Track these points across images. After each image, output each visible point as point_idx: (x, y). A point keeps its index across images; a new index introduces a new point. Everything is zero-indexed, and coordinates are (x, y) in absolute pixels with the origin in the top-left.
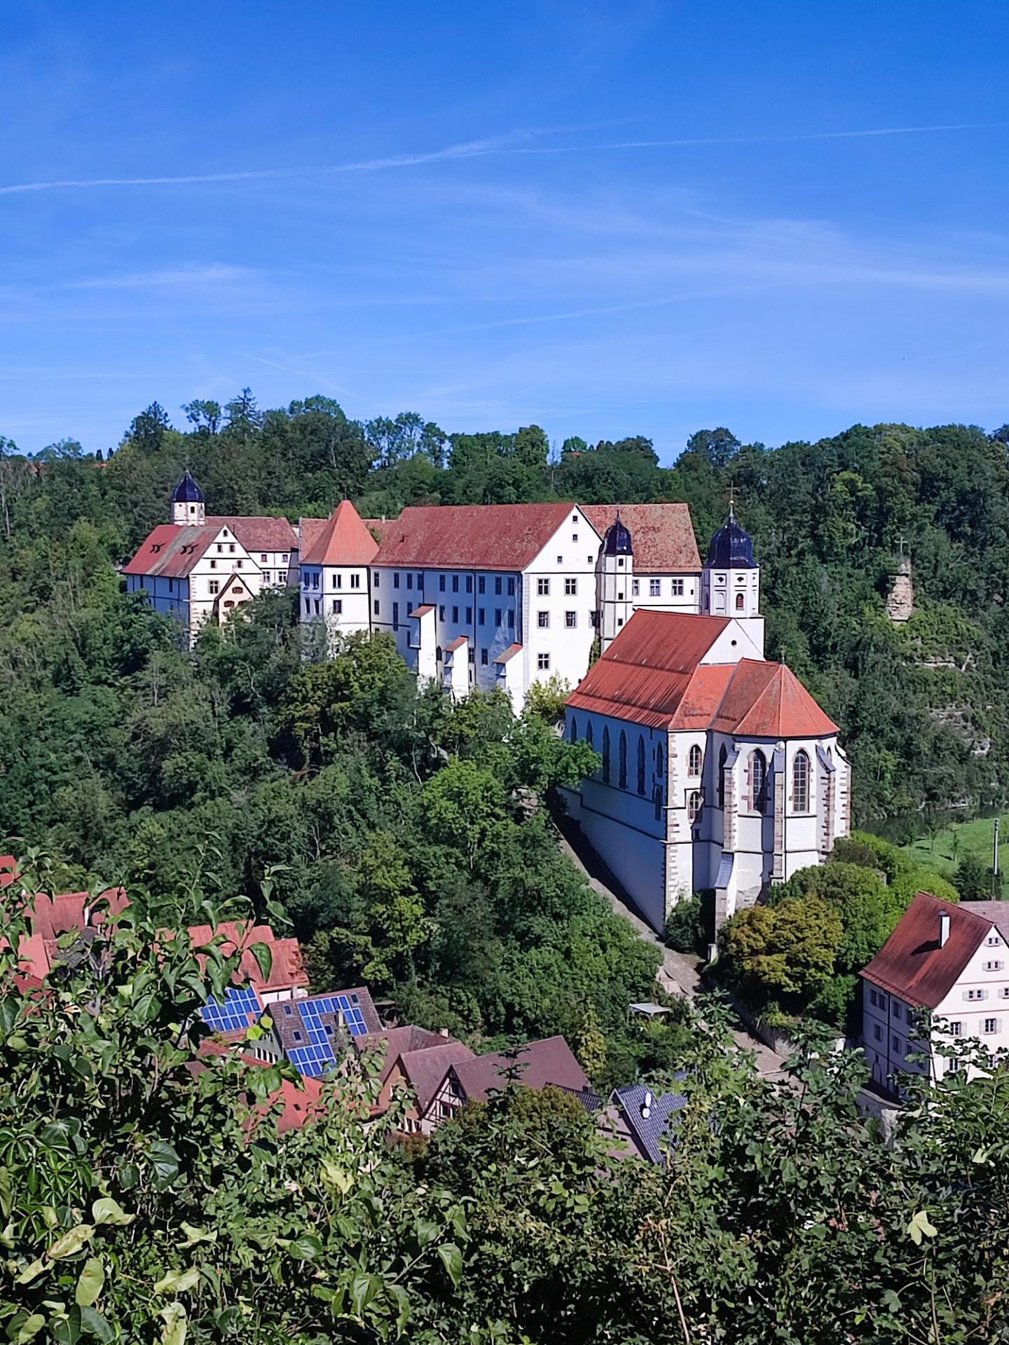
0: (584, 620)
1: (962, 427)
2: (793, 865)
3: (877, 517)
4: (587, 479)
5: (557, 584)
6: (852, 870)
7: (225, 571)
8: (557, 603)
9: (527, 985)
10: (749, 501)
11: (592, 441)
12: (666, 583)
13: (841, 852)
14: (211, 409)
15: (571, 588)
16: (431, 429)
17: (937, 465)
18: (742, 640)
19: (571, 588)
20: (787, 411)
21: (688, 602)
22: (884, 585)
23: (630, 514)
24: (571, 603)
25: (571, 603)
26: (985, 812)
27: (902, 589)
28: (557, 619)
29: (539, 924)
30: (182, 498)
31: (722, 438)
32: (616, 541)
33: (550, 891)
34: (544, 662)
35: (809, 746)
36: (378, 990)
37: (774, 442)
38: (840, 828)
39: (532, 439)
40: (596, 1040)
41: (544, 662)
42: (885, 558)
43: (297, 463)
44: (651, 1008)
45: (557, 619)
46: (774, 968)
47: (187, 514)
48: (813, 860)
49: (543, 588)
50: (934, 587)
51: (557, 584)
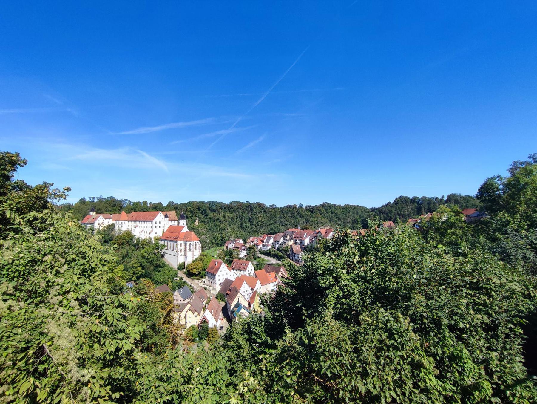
0: (161, 227)
1: (295, 207)
2: (195, 257)
3: (193, 212)
4: (156, 208)
5: (158, 223)
6: (203, 257)
7: (101, 222)
8: (158, 225)
9: (159, 278)
10: (188, 211)
11: (153, 203)
12: (173, 222)
13: (201, 255)
14: (93, 198)
15: (160, 223)
16: (129, 201)
17: (200, 206)
18: (185, 230)
19: (160, 223)
20: (181, 199)
21: (176, 224)
22: (195, 221)
23: (168, 213)
24: (160, 225)
25: (160, 225)
26: (209, 249)
27: (197, 221)
28: (158, 227)
29: (159, 269)
30: (92, 210)
31: (173, 202)
32: (166, 216)
33: (161, 264)
34: (156, 233)
35: (197, 242)
36: (135, 281)
37: (179, 203)
38: (201, 252)
39: (145, 203)
40: (170, 284)
41: (156, 233)
42: (195, 218)
43: (112, 206)
44: (177, 279)
45: (158, 227)
46: (194, 271)
47: (92, 213)
48: (198, 256)
49: (156, 223)
50: (201, 221)
51: (158, 223)
